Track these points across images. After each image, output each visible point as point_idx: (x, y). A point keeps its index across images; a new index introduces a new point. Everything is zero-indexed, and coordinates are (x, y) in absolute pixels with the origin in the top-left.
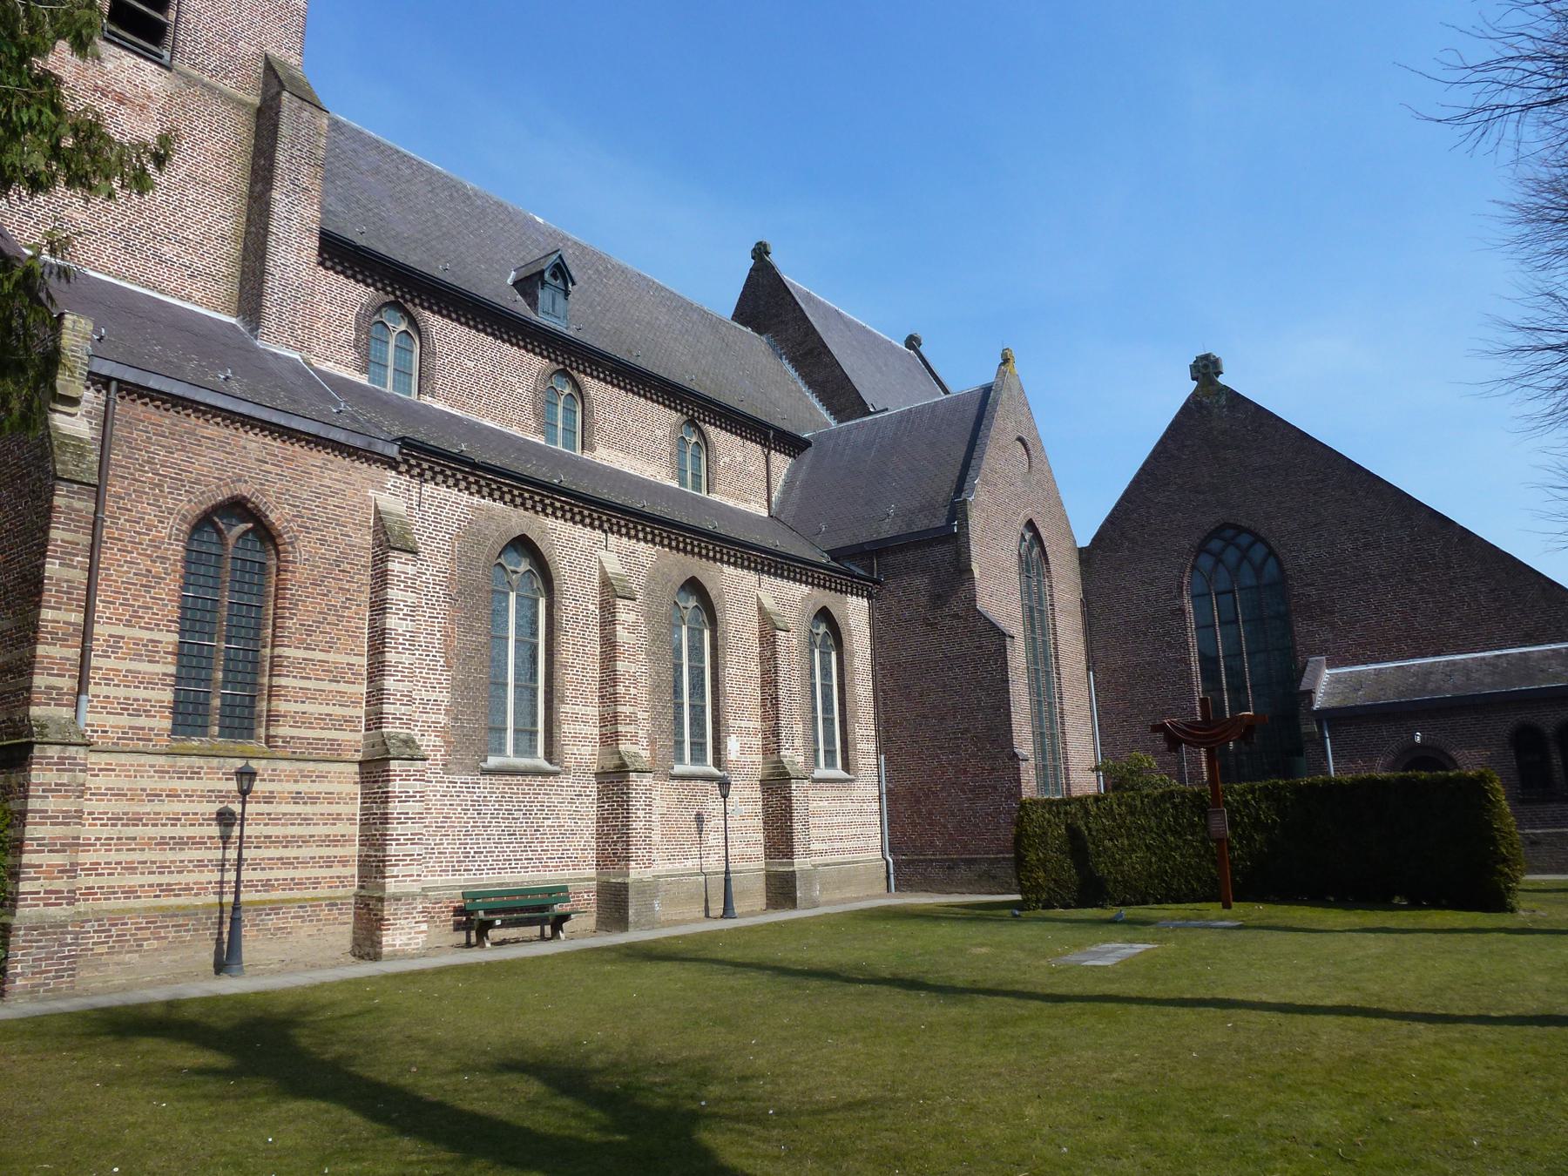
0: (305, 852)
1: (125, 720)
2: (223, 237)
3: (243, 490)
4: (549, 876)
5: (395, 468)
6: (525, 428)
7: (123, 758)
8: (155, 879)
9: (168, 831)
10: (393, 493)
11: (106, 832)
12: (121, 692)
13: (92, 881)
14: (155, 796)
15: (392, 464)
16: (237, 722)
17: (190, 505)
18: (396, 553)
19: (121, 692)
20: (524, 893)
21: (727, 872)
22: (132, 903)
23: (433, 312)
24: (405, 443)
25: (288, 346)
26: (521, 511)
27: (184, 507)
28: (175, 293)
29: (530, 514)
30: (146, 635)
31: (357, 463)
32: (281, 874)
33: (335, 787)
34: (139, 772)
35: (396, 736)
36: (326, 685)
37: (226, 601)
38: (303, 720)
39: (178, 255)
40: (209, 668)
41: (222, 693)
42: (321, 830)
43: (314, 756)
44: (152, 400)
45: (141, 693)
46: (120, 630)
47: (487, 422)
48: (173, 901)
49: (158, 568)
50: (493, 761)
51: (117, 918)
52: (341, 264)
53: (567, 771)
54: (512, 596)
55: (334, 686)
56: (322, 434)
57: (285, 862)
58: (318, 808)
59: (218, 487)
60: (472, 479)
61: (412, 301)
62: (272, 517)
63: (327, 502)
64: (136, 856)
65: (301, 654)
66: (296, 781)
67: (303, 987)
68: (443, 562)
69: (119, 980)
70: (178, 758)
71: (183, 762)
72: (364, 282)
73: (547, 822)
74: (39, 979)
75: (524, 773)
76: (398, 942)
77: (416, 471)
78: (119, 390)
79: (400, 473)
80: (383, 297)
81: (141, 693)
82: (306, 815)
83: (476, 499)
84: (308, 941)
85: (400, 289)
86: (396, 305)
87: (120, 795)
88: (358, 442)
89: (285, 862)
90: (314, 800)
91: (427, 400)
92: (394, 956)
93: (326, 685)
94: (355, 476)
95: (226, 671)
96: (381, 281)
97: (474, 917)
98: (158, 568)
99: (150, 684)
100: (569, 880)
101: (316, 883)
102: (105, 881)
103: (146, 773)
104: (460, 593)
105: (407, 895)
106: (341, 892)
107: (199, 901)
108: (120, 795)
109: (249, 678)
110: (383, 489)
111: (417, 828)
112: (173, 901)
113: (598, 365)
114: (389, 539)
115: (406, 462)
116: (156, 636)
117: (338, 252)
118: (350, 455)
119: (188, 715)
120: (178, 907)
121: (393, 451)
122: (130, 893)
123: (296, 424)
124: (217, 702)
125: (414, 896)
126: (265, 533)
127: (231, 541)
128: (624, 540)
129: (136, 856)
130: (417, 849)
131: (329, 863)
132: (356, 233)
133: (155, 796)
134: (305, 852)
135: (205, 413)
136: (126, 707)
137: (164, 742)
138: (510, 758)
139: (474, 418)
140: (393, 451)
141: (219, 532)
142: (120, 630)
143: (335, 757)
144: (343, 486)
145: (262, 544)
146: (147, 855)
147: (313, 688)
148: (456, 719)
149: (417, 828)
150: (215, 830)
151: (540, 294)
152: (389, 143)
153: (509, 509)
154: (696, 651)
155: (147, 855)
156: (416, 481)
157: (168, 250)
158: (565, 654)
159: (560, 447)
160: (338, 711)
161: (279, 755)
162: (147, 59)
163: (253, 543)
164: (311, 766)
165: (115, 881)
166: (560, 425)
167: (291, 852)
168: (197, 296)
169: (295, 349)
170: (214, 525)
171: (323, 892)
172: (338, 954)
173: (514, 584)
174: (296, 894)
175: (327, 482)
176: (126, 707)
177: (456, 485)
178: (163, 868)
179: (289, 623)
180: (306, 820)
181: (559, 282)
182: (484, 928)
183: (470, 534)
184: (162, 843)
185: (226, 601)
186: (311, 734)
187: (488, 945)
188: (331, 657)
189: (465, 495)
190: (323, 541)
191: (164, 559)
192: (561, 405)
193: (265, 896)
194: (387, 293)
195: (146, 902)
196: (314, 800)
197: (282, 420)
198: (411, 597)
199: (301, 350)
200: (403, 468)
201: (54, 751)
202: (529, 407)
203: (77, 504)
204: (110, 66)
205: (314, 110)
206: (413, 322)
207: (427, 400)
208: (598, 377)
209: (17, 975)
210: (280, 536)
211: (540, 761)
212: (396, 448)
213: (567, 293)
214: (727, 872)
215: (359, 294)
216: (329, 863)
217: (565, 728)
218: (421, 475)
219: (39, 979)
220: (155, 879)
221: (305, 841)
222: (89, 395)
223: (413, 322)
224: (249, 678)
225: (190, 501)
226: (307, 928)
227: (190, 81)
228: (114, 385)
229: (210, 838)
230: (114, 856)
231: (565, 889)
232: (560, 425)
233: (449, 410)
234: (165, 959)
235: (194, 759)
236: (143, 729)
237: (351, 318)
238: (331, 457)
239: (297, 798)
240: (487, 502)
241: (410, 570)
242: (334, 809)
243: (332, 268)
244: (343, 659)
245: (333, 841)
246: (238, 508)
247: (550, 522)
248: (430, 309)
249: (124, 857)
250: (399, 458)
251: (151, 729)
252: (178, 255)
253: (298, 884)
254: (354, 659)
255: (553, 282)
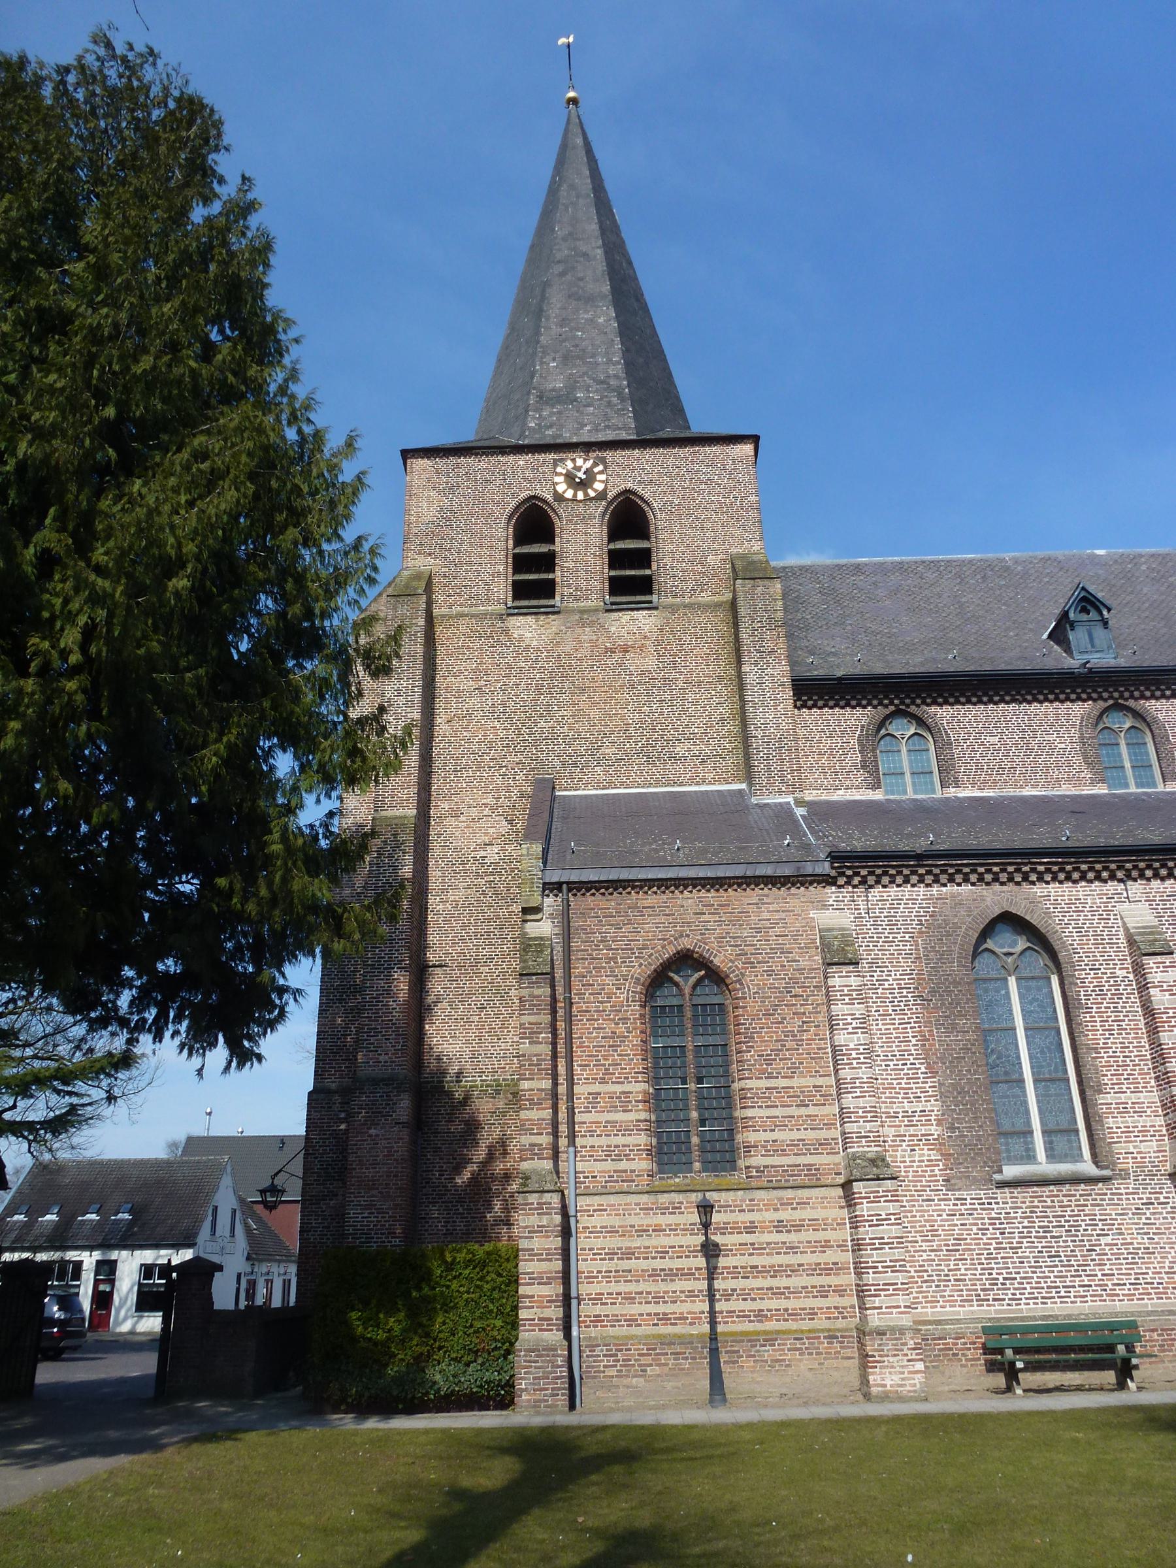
0: (795, 1282)
1: (609, 1165)
2: (723, 720)
3: (686, 943)
4: (1119, 1307)
5: (834, 883)
6: (1078, 782)
7: (612, 1199)
8: (652, 1308)
9: (658, 1264)
10: (835, 910)
11: (605, 1266)
12: (604, 1141)
13: (598, 1310)
14: (643, 1231)
15: (829, 881)
16: (718, 1157)
17: (642, 969)
18: (835, 968)
19: (604, 1141)
20: (1063, 1329)
21: (713, 1336)
22: (634, 1330)
23: (941, 705)
24: (835, 857)
25: (780, 793)
26: (997, 887)
27: (637, 971)
28: (692, 782)
29: (1011, 887)
30: (618, 1088)
31: (793, 890)
32: (774, 1304)
33: (819, 1213)
34: (627, 1211)
35: (863, 1156)
36: (794, 1111)
37: (690, 1046)
38: (777, 1149)
39: (689, 750)
40: (686, 1108)
41: (696, 1130)
42: (809, 1259)
43: (791, 1183)
44: (598, 890)
45: (620, 1140)
46: (596, 1087)
47: (1028, 792)
48: (669, 1329)
49: (621, 1029)
50: (1011, 1171)
51: (621, 1344)
52: (832, 698)
53: (1124, 1175)
54: (1012, 981)
55: (803, 1111)
56: (749, 874)
57: (777, 1293)
58: (804, 1236)
59: (663, 947)
60: (922, 871)
61: (913, 703)
62: (716, 961)
63: (764, 934)
64: (632, 1287)
65: (763, 1083)
66: (776, 1210)
67: (726, 1425)
68: (907, 964)
69: (628, 1402)
70: (659, 1196)
71: (664, 1199)
72: (859, 705)
73: (1103, 1240)
74: (539, 1396)
75: (1059, 1181)
76: (888, 1382)
77: (856, 880)
78: (569, 890)
79: (840, 887)
80: (882, 711)
81: (620, 1140)
82: (781, 1240)
83: (935, 890)
84: (809, 1375)
85: (897, 697)
86: (899, 713)
87: (613, 1232)
88: (787, 870)
89: (777, 1293)
90: (798, 1227)
91: (952, 792)
92: (885, 1397)
93: (794, 1111)
94: (793, 903)
95: (700, 1108)
96: (875, 697)
97: (1015, 1353)
98: (621, 1029)
99: (627, 1131)
100: (1140, 1314)
101: (812, 1314)
102: (608, 1310)
103: (631, 1211)
104: (933, 992)
105: (893, 1329)
106: (840, 1324)
107: (694, 1330)
108: (613, 1232)
109: (724, 1114)
110: (825, 907)
111: (897, 1254)
112: (669, 1329)
113: (1158, 684)
114: (838, 954)
115: (842, 874)
116: (627, 1087)
117: (812, 691)
118: (783, 885)
119: (668, 1153)
120: (675, 1335)
121: (825, 868)
122: (631, 1321)
123: (721, 872)
124: (695, 1140)
125: (902, 1331)
126: (716, 977)
127: (687, 991)
128: (1155, 884)
129: (632, 1287)
130: (900, 1278)
131: (823, 1292)
132: (819, 668)
133: (643, 1231)
134: (795, 1282)
135: (641, 887)
136: (610, 1153)
137: (645, 1182)
138: (1043, 1166)
139: (1011, 792)
140: (825, 868)
141: (677, 984)
142: (596, 1087)
143: (814, 1183)
144: (783, 915)
145: (718, 986)
146: (642, 1287)
147: (773, 1120)
148: (952, 1128)
149: (897, 1254)
150: (701, 1262)
151: (1071, 636)
152: (914, 558)
153: (981, 889)
154: (1041, 1028)
155: (642, 1287)
156: (860, 890)
157: (680, 750)
158: (1094, 1033)
159: (1133, 789)
160: (811, 1135)
161: (754, 1185)
162: (638, 609)
163: (710, 988)
164: (790, 1193)
165: (617, 1310)
166: (1128, 765)
167: (780, 1282)
168: (709, 776)
169: (787, 793)
170: (671, 980)
171: (821, 1323)
172: (845, 1391)
173: (1011, 968)
174: (792, 1325)
175: (765, 915)
176: (610, 1153)
177: (921, 881)
178: (658, 1298)
179: (747, 1056)
180: (792, 1249)
181: (1093, 615)
182: (1012, 1375)
183: (936, 928)
184: (654, 1274)
185: (690, 1046)
186: (785, 1161)
187: (1019, 1391)
188: (796, 1082)
189: (921, 889)
190: (770, 972)
191: (625, 1020)
192: (1123, 743)
193: (759, 1327)
194: (886, 706)
195: (646, 1330)
196: (798, 1227)
197: (709, 873)
198: (859, 1009)
199: (793, 792)
200: (842, 881)
201: (533, 1199)
202: (1078, 760)
203: (537, 992)
204: (613, 629)
205: (766, 582)
206: (920, 722)
207: (952, 792)
208: (1163, 696)
209: (522, 1390)
210: (728, 976)
211: (1087, 1167)
212: (827, 864)
213: (1105, 623)
214: (713, 1336)
215: (858, 718)
216: (823, 1292)
217: (1110, 1122)
218: (864, 882)
219: (539, 1396)
220: (652, 1308)
221: (795, 1270)
222: (549, 901)
223: (920, 722)
224: (724, 1114)
225: (641, 965)
226: (805, 1364)
227: (673, 608)
228: (565, 886)
229: (697, 1269)
230: (614, 1288)
231: (1132, 1325)
232: (1128, 765)
233: (978, 794)
234: (669, 1385)
235: (673, 1195)
236: (626, 1171)
237: (854, 743)
238: (766, 891)
239: (779, 1226)
240: (951, 889)
241: (854, 981)
242: (821, 1236)
243: (825, 706)
244: (809, 1082)
245: (827, 1270)
246: (685, 960)
247: (1039, 890)
248: (935, 703)
249: (623, 1288)
250: (833, 873)
251: (633, 1171)
252: (689, 750)
253: (793, 1315)
254: (820, 1081)
255: (1084, 617)
